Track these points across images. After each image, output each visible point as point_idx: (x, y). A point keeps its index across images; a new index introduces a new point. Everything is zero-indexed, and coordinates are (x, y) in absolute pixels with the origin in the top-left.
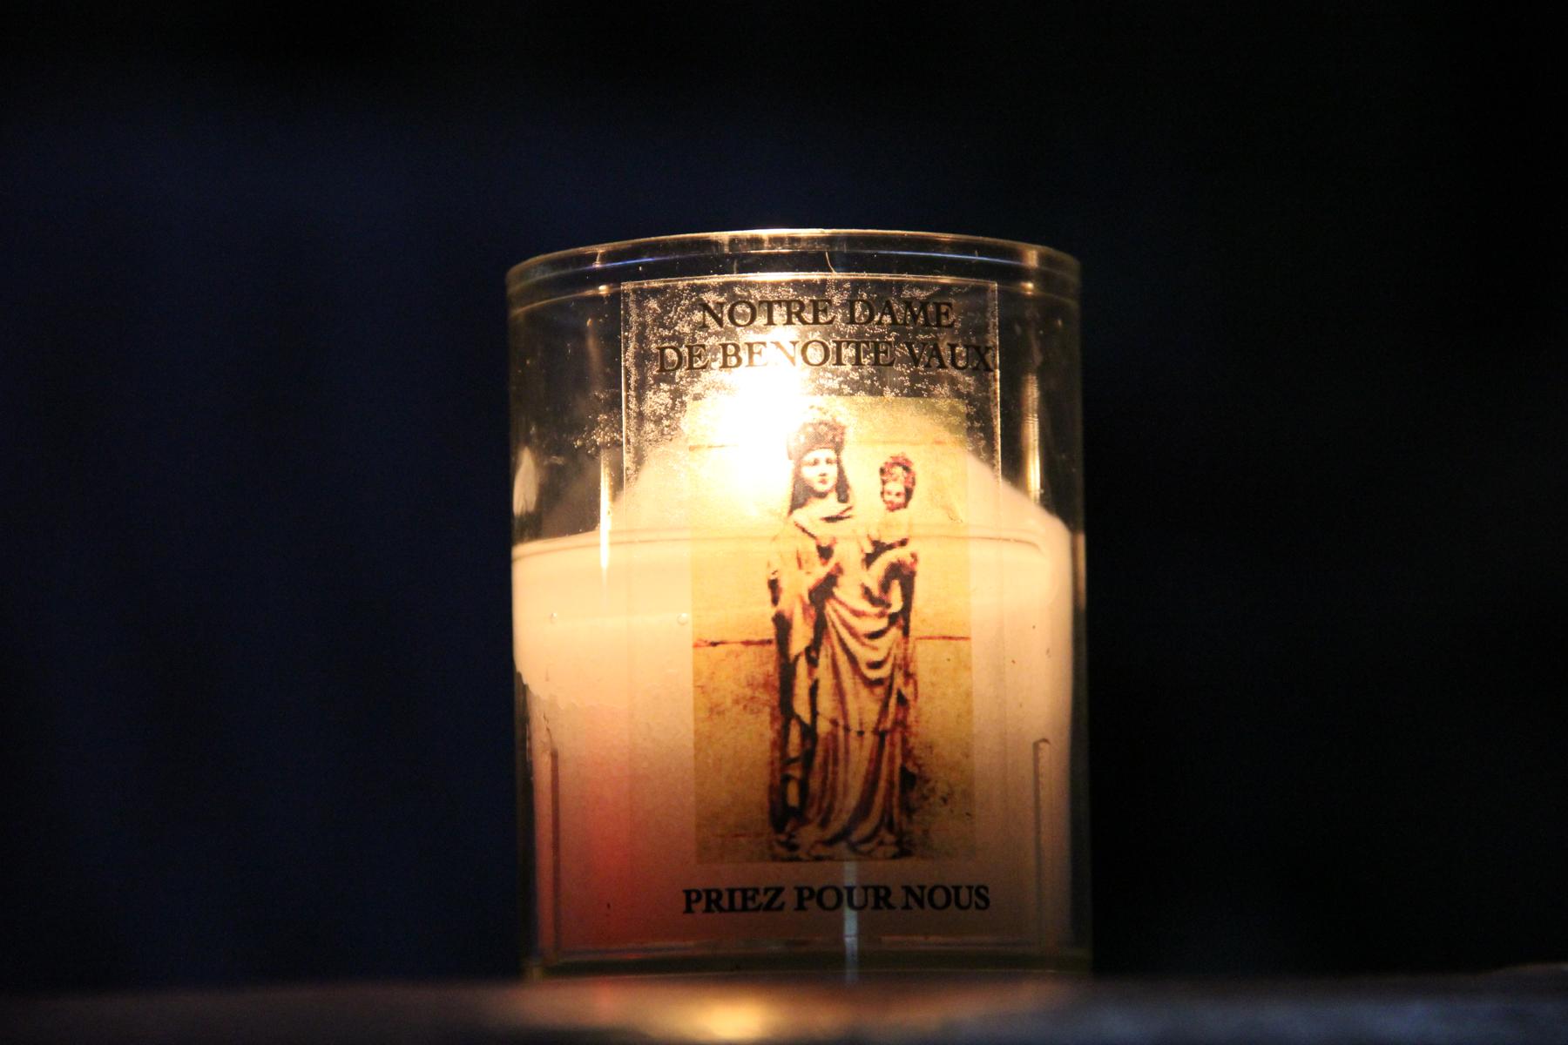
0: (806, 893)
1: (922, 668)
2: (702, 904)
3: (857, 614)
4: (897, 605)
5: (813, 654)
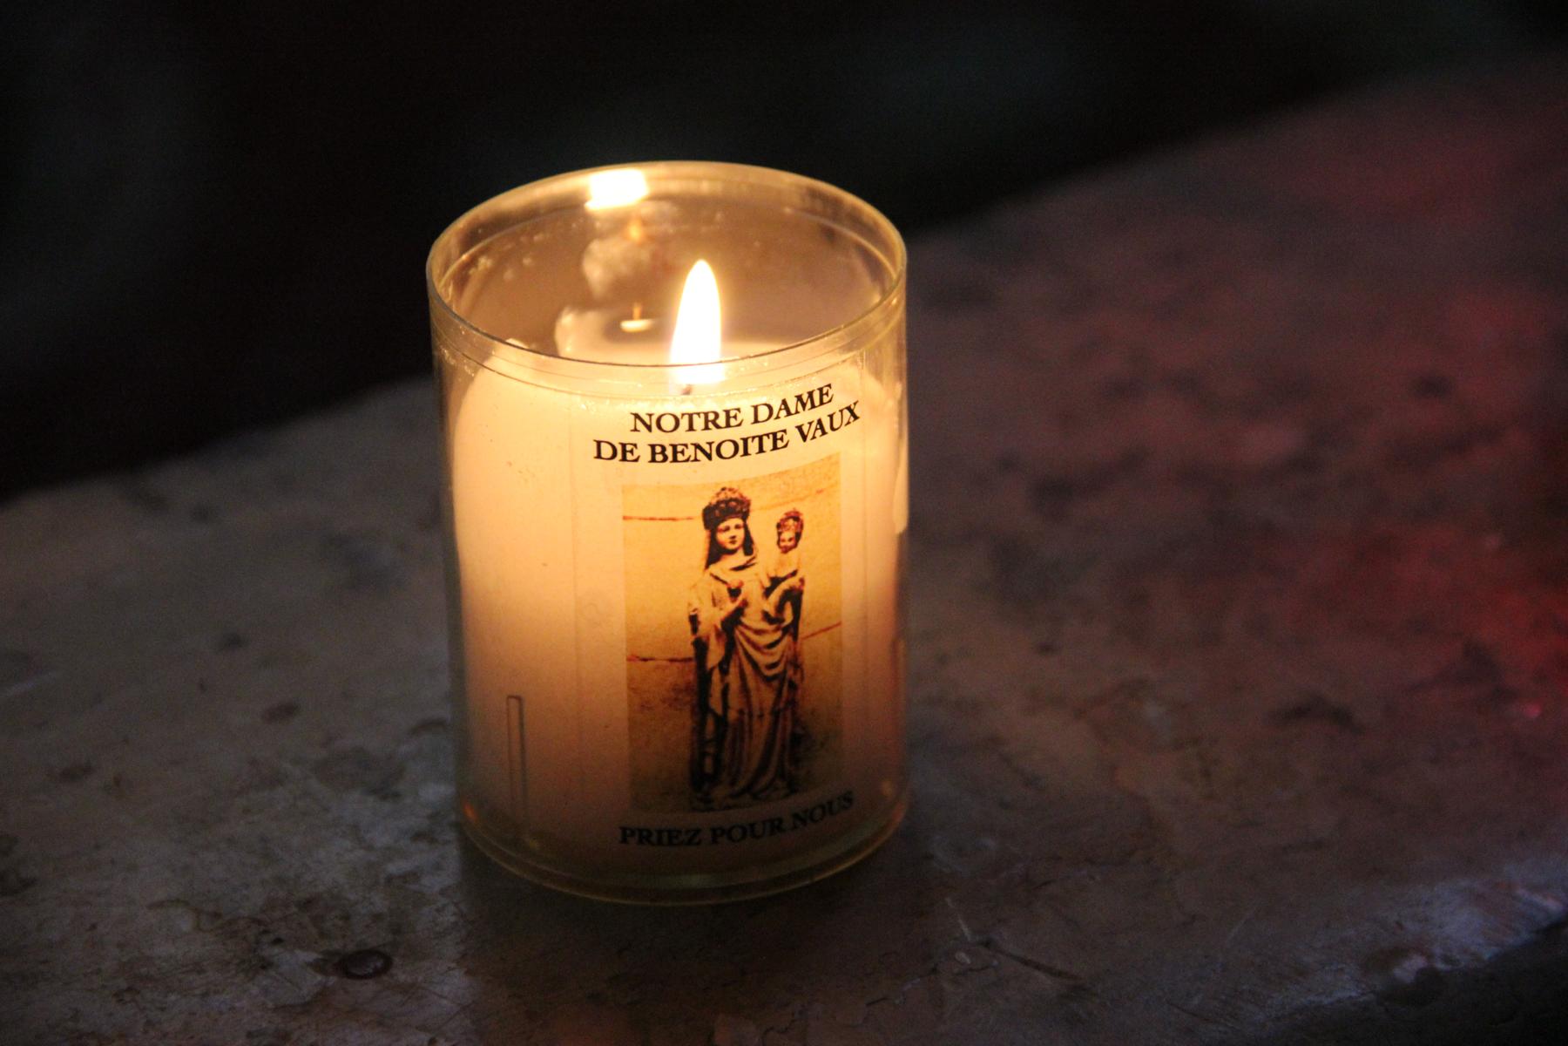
1: (807, 660)
3: (759, 632)
5: (725, 667)
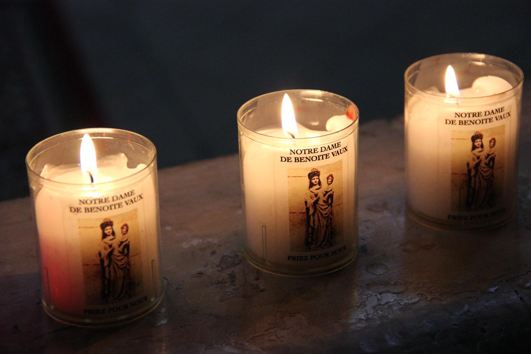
0: (313, 257)
2: (292, 259)
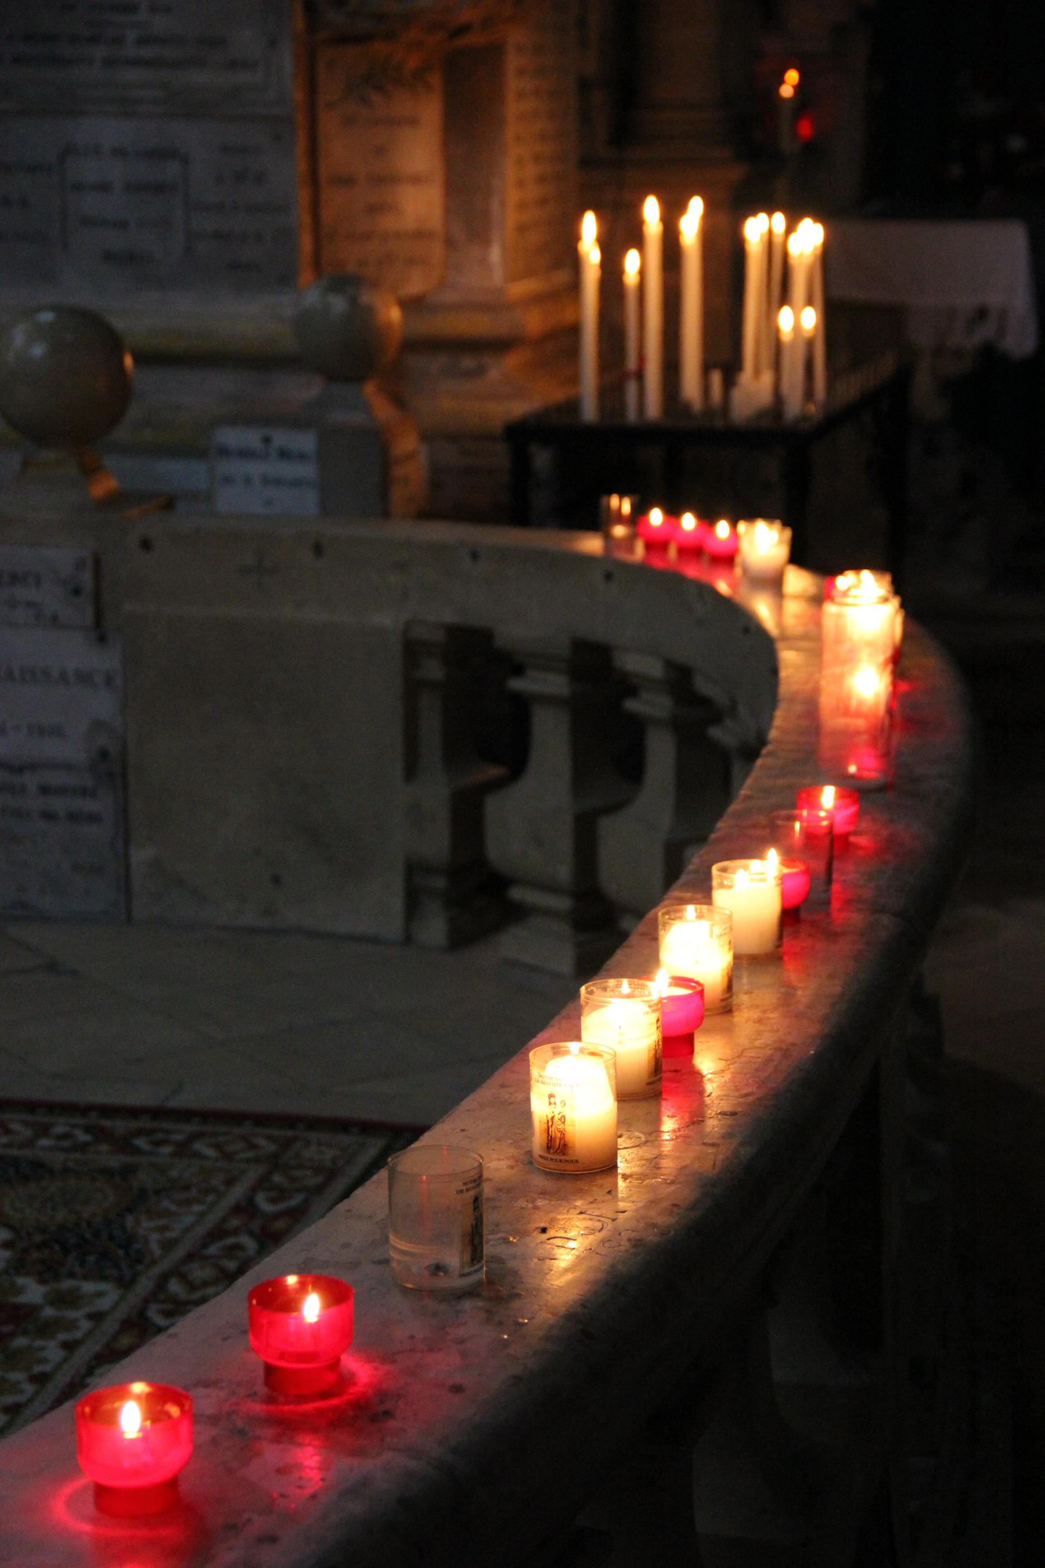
4: (563, 1120)
